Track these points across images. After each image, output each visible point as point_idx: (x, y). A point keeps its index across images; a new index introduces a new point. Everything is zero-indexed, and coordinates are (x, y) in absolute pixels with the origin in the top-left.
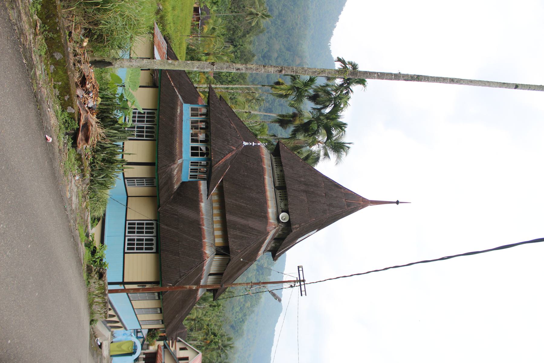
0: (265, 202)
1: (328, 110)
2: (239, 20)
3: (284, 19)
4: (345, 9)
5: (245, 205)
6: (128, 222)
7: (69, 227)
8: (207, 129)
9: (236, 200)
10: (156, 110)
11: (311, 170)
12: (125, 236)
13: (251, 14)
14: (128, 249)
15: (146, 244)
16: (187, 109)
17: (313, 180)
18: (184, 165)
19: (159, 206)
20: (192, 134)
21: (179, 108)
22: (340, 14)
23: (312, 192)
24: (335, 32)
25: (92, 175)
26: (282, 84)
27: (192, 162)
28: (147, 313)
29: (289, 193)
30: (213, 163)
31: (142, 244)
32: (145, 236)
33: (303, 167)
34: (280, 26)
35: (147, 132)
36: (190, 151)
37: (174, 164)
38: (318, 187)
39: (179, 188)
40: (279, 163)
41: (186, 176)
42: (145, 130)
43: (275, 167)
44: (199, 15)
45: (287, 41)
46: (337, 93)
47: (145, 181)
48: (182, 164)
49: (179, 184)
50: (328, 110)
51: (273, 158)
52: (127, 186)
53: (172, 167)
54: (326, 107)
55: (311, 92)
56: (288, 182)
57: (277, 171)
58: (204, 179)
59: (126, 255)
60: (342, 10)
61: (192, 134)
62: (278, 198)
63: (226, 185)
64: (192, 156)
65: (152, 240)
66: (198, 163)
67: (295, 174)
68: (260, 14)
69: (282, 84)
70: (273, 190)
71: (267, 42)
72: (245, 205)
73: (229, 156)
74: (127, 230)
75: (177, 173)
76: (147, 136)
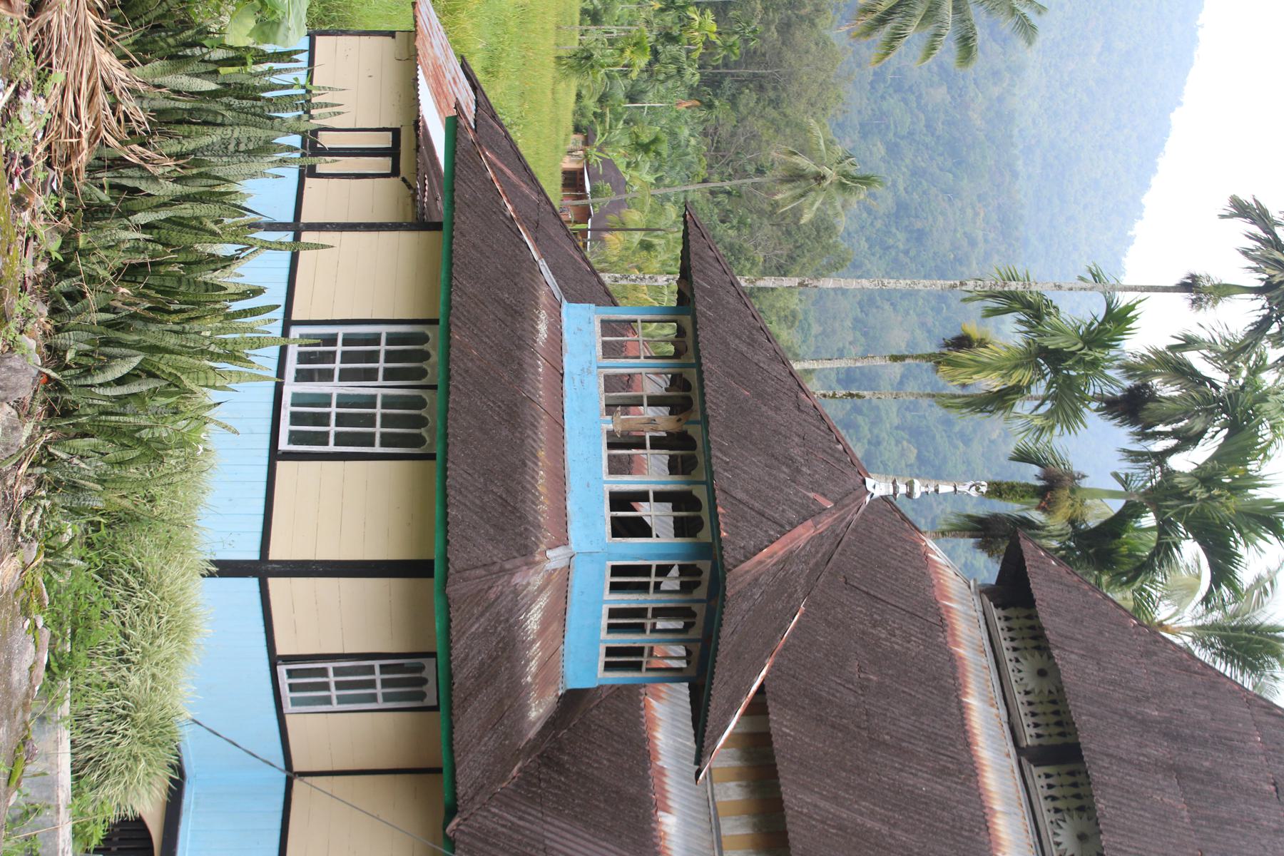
0: (981, 821)
1: (1201, 453)
2: (742, 222)
3: (919, 225)
4: (1164, 163)
5: (885, 830)
8: (683, 449)
9: (835, 799)
10: (434, 322)
11: (1187, 670)
13: (796, 176)
16: (581, 326)
17: (1203, 716)
18: (574, 589)
19: (452, 811)
20: (610, 434)
21: (543, 315)
22: (1146, 186)
23: (1208, 772)
25: (54, 354)
26: (983, 343)
27: (616, 571)
29: (1095, 775)
30: (729, 555)
33: (1147, 654)
34: (906, 252)
36: (607, 514)
37: (531, 564)
38: (1232, 750)
39: (555, 722)
40: (1033, 639)
41: (583, 662)
42: (379, 411)
43: (1008, 655)
44: (584, 197)
45: (938, 311)
46: (1234, 372)
47: (378, 677)
48: (565, 574)
49: (551, 699)
50: (1201, 453)
51: (996, 613)
52: (288, 707)
53: (518, 579)
54: (1188, 440)
55: (1117, 383)
56: (1083, 716)
57: (1022, 675)
58: (675, 675)
59: (281, 466)
60: (1154, 171)
61: (610, 434)
62: (1043, 806)
63: (781, 723)
64: (615, 533)
66: (644, 571)
67: (1112, 683)
68: (831, 174)
69: (983, 343)
70: (1013, 762)
71: (856, 320)
72: (885, 830)
73: (803, 534)
74: (285, 427)
75: (545, 624)
76: (387, 698)
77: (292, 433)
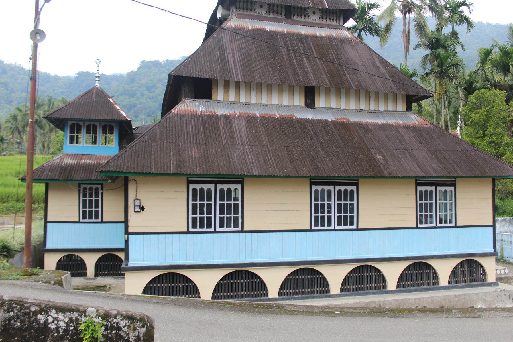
6: (314, 228)
7: (320, 312)
12: (215, 232)
14: (236, 226)
15: (346, 200)
24: (493, 22)
28: (228, 96)
31: (202, 206)
32: (215, 203)
35: (91, 196)
59: (245, 229)
65: (222, 191)
76: (97, 195)
77: (234, 227)
